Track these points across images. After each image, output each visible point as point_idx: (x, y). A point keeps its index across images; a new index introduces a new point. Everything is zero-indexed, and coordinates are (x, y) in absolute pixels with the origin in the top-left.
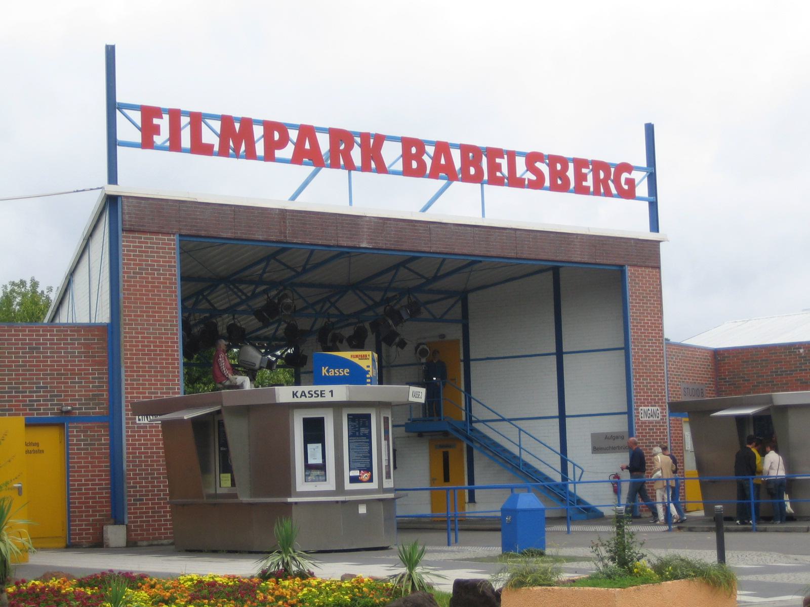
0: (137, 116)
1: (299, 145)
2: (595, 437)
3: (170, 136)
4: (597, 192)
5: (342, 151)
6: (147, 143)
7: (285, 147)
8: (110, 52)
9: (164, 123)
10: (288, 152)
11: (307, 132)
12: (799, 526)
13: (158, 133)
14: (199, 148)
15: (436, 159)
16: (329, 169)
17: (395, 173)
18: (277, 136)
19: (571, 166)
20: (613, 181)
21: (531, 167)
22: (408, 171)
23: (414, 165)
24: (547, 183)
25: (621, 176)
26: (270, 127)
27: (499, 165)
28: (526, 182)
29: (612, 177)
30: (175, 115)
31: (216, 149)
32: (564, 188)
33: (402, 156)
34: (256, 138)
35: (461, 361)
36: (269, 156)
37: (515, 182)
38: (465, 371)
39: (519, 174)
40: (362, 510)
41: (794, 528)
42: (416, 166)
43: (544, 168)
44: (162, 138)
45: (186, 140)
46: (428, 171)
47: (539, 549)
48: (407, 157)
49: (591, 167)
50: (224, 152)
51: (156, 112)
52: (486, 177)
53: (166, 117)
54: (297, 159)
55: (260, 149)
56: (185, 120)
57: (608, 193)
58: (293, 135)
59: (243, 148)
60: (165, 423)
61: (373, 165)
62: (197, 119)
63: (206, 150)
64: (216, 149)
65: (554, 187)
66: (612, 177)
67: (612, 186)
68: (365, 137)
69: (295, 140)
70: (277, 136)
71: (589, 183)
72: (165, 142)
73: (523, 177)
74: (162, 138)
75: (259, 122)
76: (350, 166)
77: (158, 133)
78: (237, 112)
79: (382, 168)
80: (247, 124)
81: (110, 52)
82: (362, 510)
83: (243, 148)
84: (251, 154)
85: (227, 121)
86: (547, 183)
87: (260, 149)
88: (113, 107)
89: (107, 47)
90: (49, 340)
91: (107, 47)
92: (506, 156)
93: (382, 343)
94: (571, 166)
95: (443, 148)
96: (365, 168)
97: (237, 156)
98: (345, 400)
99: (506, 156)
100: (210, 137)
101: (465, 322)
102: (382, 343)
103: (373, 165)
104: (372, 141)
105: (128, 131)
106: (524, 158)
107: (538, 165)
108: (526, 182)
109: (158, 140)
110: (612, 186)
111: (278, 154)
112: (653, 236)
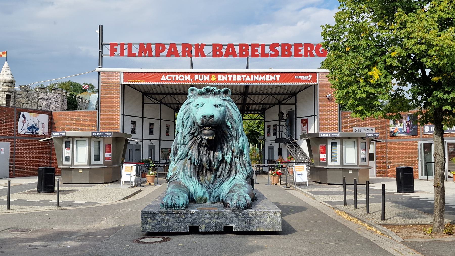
0: (109, 46)
1: (170, 50)
2: (421, 176)
4: (306, 55)
9: (118, 48)
11: (173, 46)
14: (131, 54)
15: (227, 50)
17: (210, 56)
18: (161, 48)
19: (293, 47)
21: (277, 52)
22: (215, 55)
23: (218, 53)
26: (158, 45)
28: (270, 55)
29: (315, 49)
30: (122, 45)
31: (137, 54)
32: (290, 55)
36: (157, 55)
37: (264, 55)
39: (266, 52)
43: (279, 49)
44: (118, 52)
45: (126, 52)
47: (436, 227)
48: (214, 51)
49: (303, 46)
50: (140, 55)
51: (116, 44)
53: (119, 46)
54: (168, 55)
55: (154, 53)
56: (126, 47)
57: (312, 55)
58: (167, 47)
59: (147, 54)
60: (141, 145)
62: (130, 45)
63: (134, 55)
64: (137, 54)
65: (284, 55)
66: (315, 49)
67: (314, 52)
68: (197, 45)
70: (161, 48)
71: (302, 52)
74: (118, 52)
79: (203, 55)
80: (149, 45)
81: (101, 28)
83: (147, 54)
84: (150, 55)
85: (141, 45)
86: (280, 54)
87: (154, 53)
88: (101, 46)
92: (260, 46)
93: (6, 64)
94: (293, 47)
95: (231, 46)
96: (197, 56)
97: (145, 56)
98: (396, 182)
99: (260, 46)
100: (135, 50)
102: (6, 64)
104: (200, 46)
105: (106, 50)
107: (276, 48)
108: (270, 55)
110: (314, 52)
111: (161, 54)
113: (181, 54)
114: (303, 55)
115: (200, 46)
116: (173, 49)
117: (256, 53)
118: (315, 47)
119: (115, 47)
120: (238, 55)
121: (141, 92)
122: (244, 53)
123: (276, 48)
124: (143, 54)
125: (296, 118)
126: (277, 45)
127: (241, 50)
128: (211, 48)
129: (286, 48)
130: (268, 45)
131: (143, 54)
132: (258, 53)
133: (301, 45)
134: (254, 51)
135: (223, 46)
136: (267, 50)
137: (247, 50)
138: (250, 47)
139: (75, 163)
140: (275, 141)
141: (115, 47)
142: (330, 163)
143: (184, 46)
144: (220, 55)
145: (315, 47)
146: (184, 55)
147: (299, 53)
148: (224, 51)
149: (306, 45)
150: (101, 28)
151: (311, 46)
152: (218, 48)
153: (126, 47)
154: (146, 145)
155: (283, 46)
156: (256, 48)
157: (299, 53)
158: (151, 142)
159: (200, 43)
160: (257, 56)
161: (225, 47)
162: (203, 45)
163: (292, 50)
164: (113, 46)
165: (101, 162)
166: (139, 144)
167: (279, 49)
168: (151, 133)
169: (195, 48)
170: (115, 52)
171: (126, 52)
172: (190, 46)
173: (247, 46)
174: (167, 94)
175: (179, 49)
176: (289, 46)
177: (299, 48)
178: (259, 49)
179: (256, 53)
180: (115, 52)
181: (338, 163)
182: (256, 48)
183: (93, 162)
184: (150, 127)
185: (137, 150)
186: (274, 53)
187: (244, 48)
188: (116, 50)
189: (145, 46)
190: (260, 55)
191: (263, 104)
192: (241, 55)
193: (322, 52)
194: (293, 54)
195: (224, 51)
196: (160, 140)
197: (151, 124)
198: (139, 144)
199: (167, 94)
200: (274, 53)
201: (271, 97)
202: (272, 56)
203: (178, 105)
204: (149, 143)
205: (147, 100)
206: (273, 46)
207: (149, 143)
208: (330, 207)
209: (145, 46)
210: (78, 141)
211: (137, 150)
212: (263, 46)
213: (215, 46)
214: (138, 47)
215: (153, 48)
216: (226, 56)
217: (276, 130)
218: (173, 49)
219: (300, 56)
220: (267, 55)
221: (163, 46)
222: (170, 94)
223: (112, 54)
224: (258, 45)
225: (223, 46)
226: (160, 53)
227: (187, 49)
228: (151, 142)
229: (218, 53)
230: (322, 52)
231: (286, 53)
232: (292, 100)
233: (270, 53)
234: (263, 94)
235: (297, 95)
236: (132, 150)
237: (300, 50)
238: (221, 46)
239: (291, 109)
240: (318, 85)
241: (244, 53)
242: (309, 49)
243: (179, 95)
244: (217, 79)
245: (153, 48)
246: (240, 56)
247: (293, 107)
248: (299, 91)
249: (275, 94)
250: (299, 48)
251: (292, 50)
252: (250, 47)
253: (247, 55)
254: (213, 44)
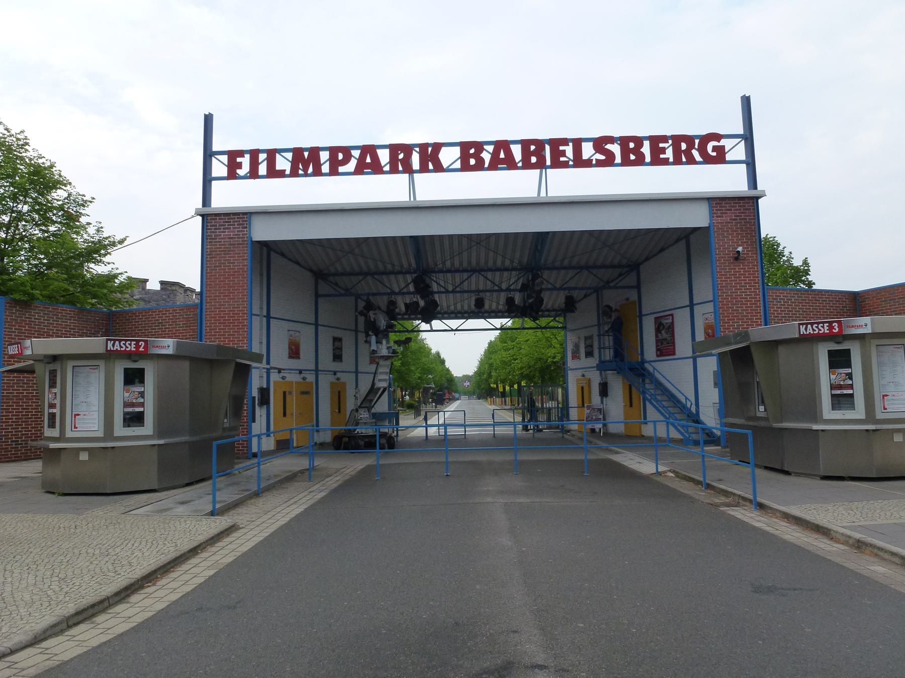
0: (224, 158)
3: (321, 168)
4: (677, 161)
5: (401, 160)
6: (232, 175)
7: (349, 163)
8: (746, 102)
9: (245, 161)
10: (351, 166)
11: (369, 150)
12: (183, 438)
13: (240, 168)
14: (273, 173)
15: (495, 155)
16: (434, 173)
18: (341, 156)
19: (647, 144)
20: (698, 150)
21: (610, 156)
22: (465, 167)
23: (472, 162)
24: (618, 160)
25: (707, 147)
26: (334, 151)
27: (563, 153)
28: (594, 162)
29: (696, 146)
30: (254, 154)
31: (288, 172)
32: (640, 161)
33: (460, 158)
34: (328, 163)
35: (264, 316)
36: (334, 172)
38: (640, 334)
39: (585, 156)
40: (84, 456)
41: (820, 465)
42: (650, 160)
43: (615, 148)
44: (245, 170)
45: (263, 169)
46: (486, 165)
48: (464, 158)
49: (670, 142)
50: (294, 173)
52: (548, 163)
53: (247, 156)
54: (359, 171)
55: (325, 168)
56: (262, 156)
57: (691, 161)
58: (356, 153)
59: (310, 170)
61: (431, 167)
62: (272, 154)
63: (281, 174)
64: (288, 172)
65: (626, 162)
66: (696, 146)
67: (695, 153)
68: (423, 147)
69: (357, 157)
70: (341, 156)
71: (669, 154)
72: (247, 173)
73: (591, 158)
74: (245, 170)
75: (324, 149)
76: (408, 170)
77: (240, 168)
78: (306, 143)
79: (439, 168)
80: (315, 152)
81: (208, 120)
82: (84, 456)
83: (310, 170)
84: (318, 172)
85: (297, 153)
86: (618, 160)
87: (325, 168)
88: (209, 155)
89: (206, 115)
90: (237, 338)
91: (206, 115)
94: (647, 144)
95: (502, 145)
96: (424, 169)
97: (306, 175)
99: (571, 144)
100: (283, 163)
101: (638, 287)
103: (431, 167)
104: (430, 149)
105: (219, 168)
106: (520, 146)
107: (609, 147)
108: (594, 162)
109: (241, 172)
110: (695, 153)
111: (341, 169)
112: (753, 193)
113: (387, 168)
114: (671, 160)
115: (430, 149)
116: (368, 156)
117: (562, 159)
118: (697, 141)
119: (239, 160)
120: (520, 165)
121: (311, 270)
122: (534, 159)
123: (609, 147)
124: (301, 172)
125: (641, 316)
126: (611, 140)
127: (526, 154)
128: (456, 152)
129: (632, 145)
130: (587, 140)
131: (301, 172)
132: (567, 159)
133: (664, 139)
134: (557, 154)
135: (485, 147)
136: (588, 151)
137: (540, 153)
138: (547, 148)
139: (69, 434)
140: (595, 369)
141: (239, 160)
142: (827, 412)
143: (394, 149)
144: (479, 166)
145: (697, 141)
146: (394, 170)
147: (662, 156)
148: (486, 157)
149: (677, 140)
150: (208, 120)
151: (689, 140)
152: (472, 151)
153: (262, 156)
154: (325, 382)
155: (624, 141)
156: (561, 148)
157: (662, 156)
158: (336, 377)
159: (431, 141)
160: (565, 165)
161: (490, 148)
162: (437, 147)
163: (646, 149)
164: (233, 156)
165: (148, 427)
166: (308, 380)
167: (615, 148)
168: (337, 357)
169: (420, 153)
170: (238, 171)
171: (263, 169)
172: (407, 149)
173: (540, 144)
174: (366, 274)
175: (384, 156)
176: (639, 141)
177: (661, 145)
178: (569, 150)
179: (562, 159)
180: (238, 171)
181: (859, 412)
182: (561, 148)
183: (120, 430)
184: (334, 345)
185: (303, 393)
186: (602, 157)
187: (533, 148)
188: (239, 165)
189: (306, 154)
190: (571, 163)
191: (569, 289)
192: (527, 165)
193: (714, 154)
194: (648, 159)
195: (486, 157)
196: (357, 372)
197: (337, 340)
198: (308, 380)
199: (366, 274)
200: (602, 157)
201: (586, 273)
202: (600, 163)
203: (390, 296)
204: (332, 378)
205: (324, 288)
206: (600, 143)
207: (332, 378)
208: (92, 268)
209: (306, 154)
210: (77, 369)
211: (303, 393)
212: (577, 143)
213: (465, 147)
214: (289, 155)
215: (324, 156)
216: (494, 166)
217: (591, 346)
218: (368, 156)
219: (666, 162)
220: (588, 164)
221: (347, 151)
222: (372, 274)
223: (232, 175)
224: (565, 142)
225: (485, 147)
226: (339, 167)
227: (401, 156)
228: (336, 377)
229: (472, 162)
230: (714, 154)
231: (632, 157)
232: (631, 279)
233: (594, 158)
234: (570, 267)
235: (642, 268)
236: (290, 393)
237: (663, 150)
238: (479, 146)
239: (627, 299)
240: (712, 228)
241: (534, 159)
242: (684, 146)
243: (392, 277)
244: (445, 429)
245: (324, 156)
246: (523, 168)
247: (633, 296)
248: (647, 259)
249: (595, 267)
250: (661, 145)
251: (646, 149)
252: (547, 148)
253: (540, 165)
254: (461, 142)
